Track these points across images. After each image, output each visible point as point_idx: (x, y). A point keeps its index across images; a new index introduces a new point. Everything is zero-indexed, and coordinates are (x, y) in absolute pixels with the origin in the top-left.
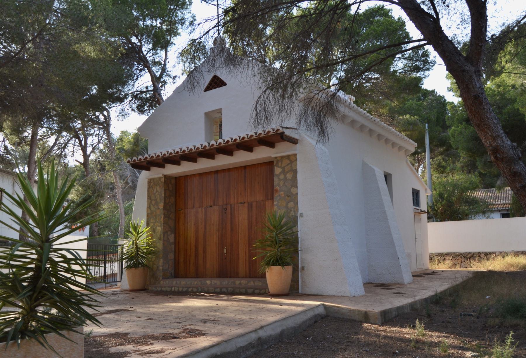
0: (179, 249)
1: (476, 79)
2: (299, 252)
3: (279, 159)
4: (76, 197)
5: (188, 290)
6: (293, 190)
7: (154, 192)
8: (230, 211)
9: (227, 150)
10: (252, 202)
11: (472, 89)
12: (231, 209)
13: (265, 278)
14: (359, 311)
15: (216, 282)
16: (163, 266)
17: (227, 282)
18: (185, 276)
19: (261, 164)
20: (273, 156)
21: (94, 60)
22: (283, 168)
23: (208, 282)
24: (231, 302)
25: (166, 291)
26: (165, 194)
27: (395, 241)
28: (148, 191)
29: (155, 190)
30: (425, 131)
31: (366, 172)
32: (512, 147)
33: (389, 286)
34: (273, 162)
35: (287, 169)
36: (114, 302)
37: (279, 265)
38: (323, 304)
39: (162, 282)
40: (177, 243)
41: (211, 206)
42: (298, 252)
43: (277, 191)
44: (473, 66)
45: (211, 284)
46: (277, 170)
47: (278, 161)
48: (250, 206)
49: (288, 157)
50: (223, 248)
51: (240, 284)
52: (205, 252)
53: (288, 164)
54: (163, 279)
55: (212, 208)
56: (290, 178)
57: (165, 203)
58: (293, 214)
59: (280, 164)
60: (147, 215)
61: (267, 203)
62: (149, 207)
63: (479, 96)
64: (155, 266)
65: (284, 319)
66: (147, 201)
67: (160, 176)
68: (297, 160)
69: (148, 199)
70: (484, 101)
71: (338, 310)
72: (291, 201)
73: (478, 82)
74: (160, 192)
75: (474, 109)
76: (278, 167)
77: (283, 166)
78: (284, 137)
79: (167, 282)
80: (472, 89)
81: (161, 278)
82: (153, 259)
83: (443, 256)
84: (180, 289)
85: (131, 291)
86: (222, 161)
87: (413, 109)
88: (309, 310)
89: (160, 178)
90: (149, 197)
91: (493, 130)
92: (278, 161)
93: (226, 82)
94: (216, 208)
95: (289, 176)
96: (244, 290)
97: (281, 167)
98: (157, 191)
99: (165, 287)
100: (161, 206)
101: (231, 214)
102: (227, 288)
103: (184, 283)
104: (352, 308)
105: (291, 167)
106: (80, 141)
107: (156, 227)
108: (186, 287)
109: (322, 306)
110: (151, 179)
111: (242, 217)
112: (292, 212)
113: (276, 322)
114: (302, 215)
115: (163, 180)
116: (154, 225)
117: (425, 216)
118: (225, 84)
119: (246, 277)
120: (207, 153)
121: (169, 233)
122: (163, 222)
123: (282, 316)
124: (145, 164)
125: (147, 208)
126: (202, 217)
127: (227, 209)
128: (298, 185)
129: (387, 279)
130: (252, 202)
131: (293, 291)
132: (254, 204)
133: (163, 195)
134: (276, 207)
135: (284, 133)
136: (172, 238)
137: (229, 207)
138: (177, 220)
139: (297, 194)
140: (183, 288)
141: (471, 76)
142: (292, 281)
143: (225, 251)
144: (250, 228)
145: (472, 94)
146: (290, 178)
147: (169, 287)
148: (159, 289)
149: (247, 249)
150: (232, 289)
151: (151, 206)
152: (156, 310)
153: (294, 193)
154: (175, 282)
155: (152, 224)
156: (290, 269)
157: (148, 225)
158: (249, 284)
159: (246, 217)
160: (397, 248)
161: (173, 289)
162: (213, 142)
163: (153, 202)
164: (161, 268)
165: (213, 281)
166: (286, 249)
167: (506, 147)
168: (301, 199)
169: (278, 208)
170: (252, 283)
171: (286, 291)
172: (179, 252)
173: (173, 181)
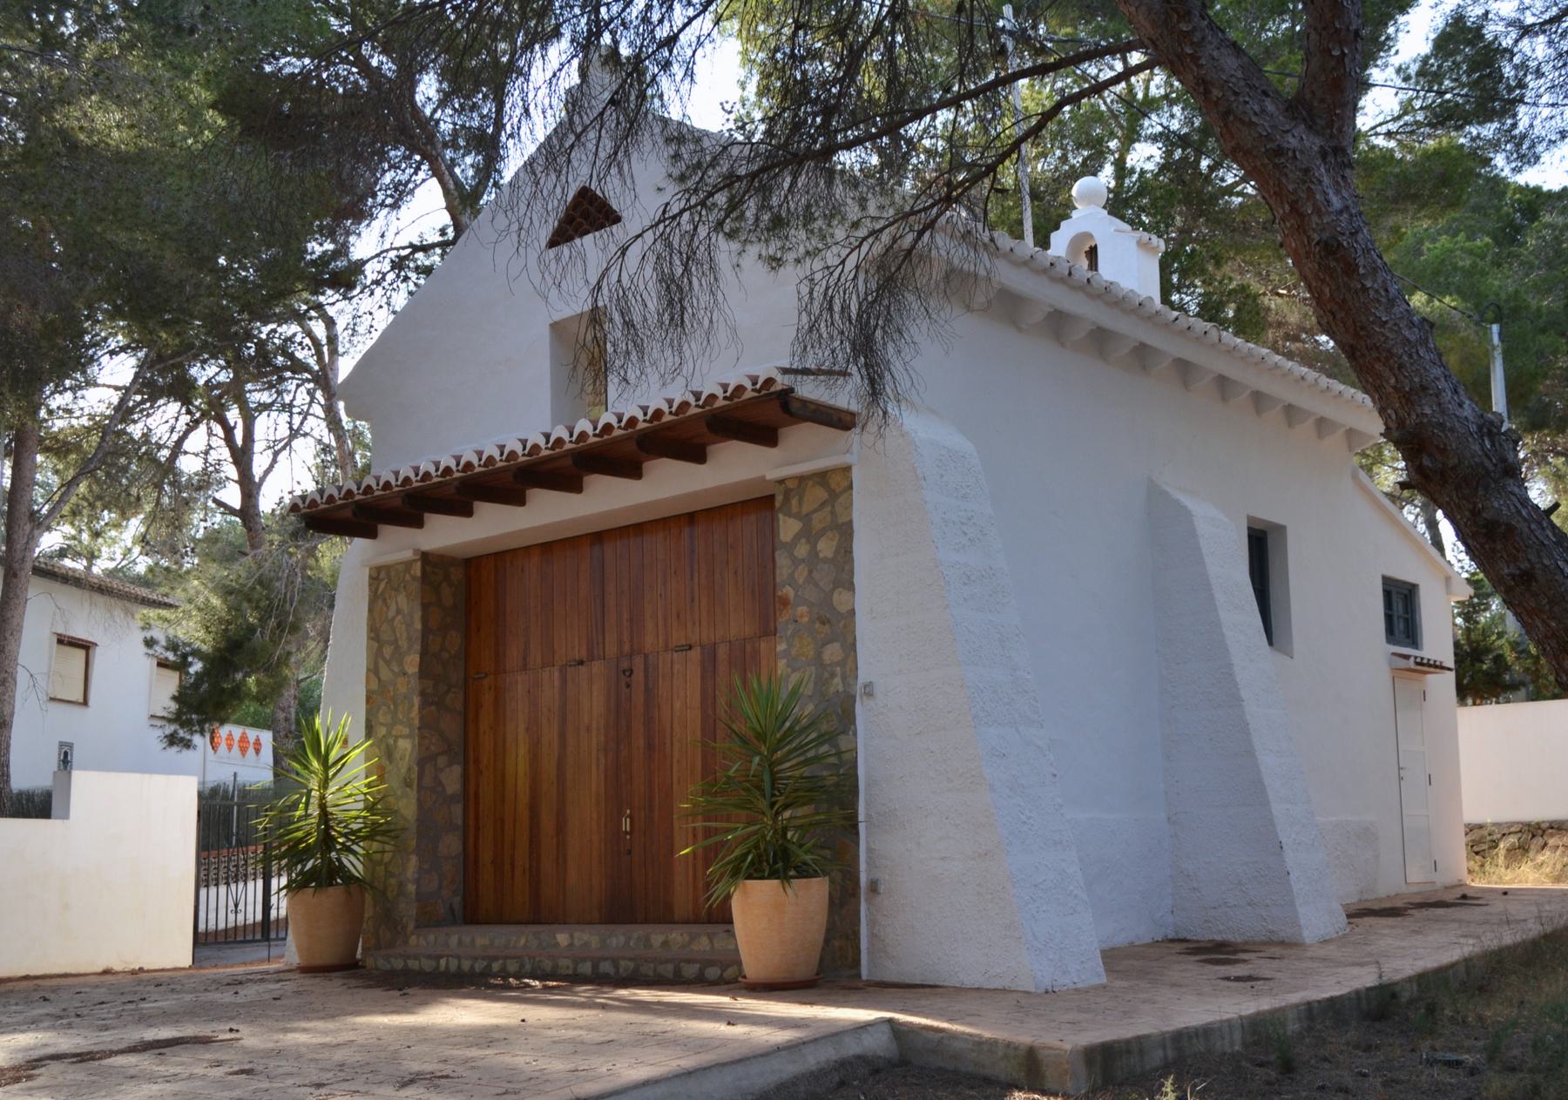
0: (477, 819)
1: (1326, 180)
2: (862, 827)
3: (790, 484)
4: (201, 634)
5: (489, 966)
6: (840, 599)
7: (391, 614)
9: (622, 454)
11: (1315, 219)
12: (646, 669)
13: (731, 922)
14: (1009, 1045)
15: (586, 937)
16: (417, 882)
17: (622, 939)
19: (744, 503)
20: (773, 474)
21: (120, 158)
22: (806, 519)
23: (562, 938)
24: (601, 1014)
25: (421, 973)
27: (1267, 781)
28: (371, 610)
29: (393, 608)
30: (1488, 355)
31: (1165, 526)
32: (1480, 428)
33: (1236, 952)
34: (771, 498)
35: (818, 521)
36: (167, 1017)
37: (773, 875)
38: (890, 1021)
39: (413, 940)
40: (469, 797)
41: (581, 663)
42: (855, 826)
43: (785, 602)
44: (1317, 133)
45: (571, 945)
46: (788, 528)
47: (787, 494)
49: (822, 477)
50: (620, 814)
51: (665, 944)
52: (561, 830)
53: (823, 505)
54: (417, 927)
55: (583, 669)
56: (830, 554)
57: (424, 654)
58: (841, 689)
59: (794, 502)
62: (373, 671)
63: (1340, 245)
64: (393, 881)
65: (689, 1074)
66: (369, 648)
67: (408, 555)
68: (851, 487)
69: (369, 638)
70: (1361, 261)
71: (940, 1041)
73: (1337, 192)
74: (407, 609)
75: (1327, 291)
76: (790, 515)
77: (805, 510)
78: (795, 406)
79: (431, 938)
80: (1315, 219)
81: (411, 926)
82: (387, 857)
83: (1532, 836)
84: (466, 965)
85: (307, 970)
86: (607, 498)
87: (1456, 268)
88: (815, 1040)
89: (408, 565)
90: (374, 633)
91: (1401, 367)
92: (787, 494)
94: (597, 667)
95: (826, 547)
96: (670, 967)
97: (797, 516)
99: (416, 957)
100: (412, 663)
101: (647, 689)
102: (615, 962)
103: (480, 941)
104: (987, 1034)
105: (833, 513)
106: (229, 431)
107: (397, 738)
108: (484, 958)
109: (886, 1028)
110: (379, 569)
112: (837, 680)
113: (646, 1084)
114: (869, 691)
115: (417, 570)
116: (389, 733)
117: (1445, 684)
120: (560, 469)
121: (442, 761)
122: (416, 722)
123: (688, 1062)
124: (348, 513)
126: (554, 705)
128: (856, 580)
129: (1236, 925)
131: (833, 968)
132: (722, 651)
133: (418, 626)
134: (782, 664)
135: (791, 390)
136: (452, 779)
137: (638, 663)
138: (469, 715)
139: (852, 612)
140: (476, 959)
141: (1306, 171)
142: (831, 931)
143: (626, 825)
145: (1316, 237)
146: (830, 554)
147: (429, 957)
148: (398, 964)
150: (631, 965)
151: (381, 663)
152: (302, 1038)
153: (843, 609)
154: (454, 940)
155: (382, 731)
156: (814, 893)
157: (370, 731)
158: (695, 947)
159: (695, 699)
160: (1277, 809)
161: (443, 962)
162: (583, 425)
164: (411, 888)
165: (577, 934)
166: (804, 812)
167: (1452, 430)
168: (864, 628)
169: (788, 666)
170: (704, 940)
171: (805, 971)
172: (477, 829)
173: (457, 574)
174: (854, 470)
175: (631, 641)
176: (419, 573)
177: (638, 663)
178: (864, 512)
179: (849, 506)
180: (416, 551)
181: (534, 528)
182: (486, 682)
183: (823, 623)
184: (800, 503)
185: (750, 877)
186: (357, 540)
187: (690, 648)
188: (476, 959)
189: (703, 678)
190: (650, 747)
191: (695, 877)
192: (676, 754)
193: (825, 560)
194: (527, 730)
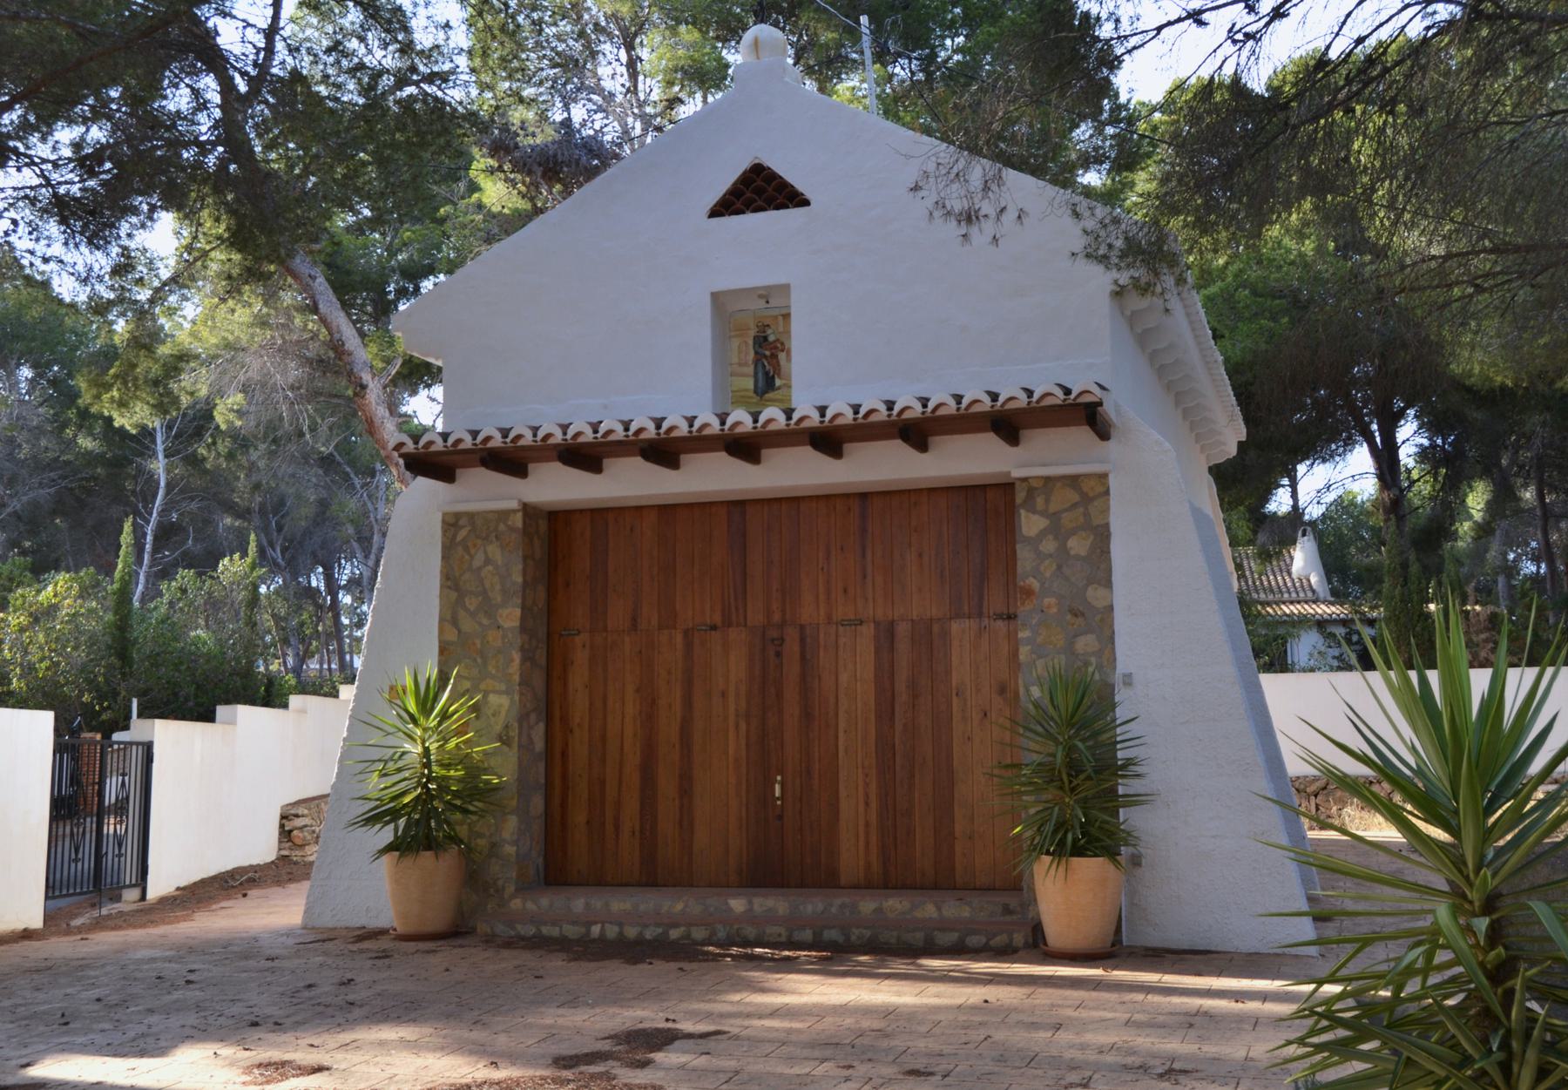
3: (1034, 484)
5: (666, 933)
6: (1095, 595)
8: (797, 648)
10: (892, 623)
12: (802, 640)
17: (820, 907)
18: (599, 880)
19: (948, 488)
20: (1017, 473)
22: (1055, 517)
26: (524, 573)
35: (1067, 520)
41: (714, 628)
43: (1028, 593)
46: (1030, 524)
47: (1031, 492)
48: (886, 634)
49: (1073, 481)
53: (1075, 506)
59: (1040, 501)
60: (442, 651)
62: (450, 619)
64: (482, 842)
67: (514, 505)
68: (1107, 492)
72: (1086, 633)
74: (504, 567)
76: (1034, 512)
77: (1053, 508)
79: (545, 902)
81: (511, 889)
84: (631, 932)
89: (504, 515)
92: (1031, 492)
93: (808, 195)
95: (1078, 545)
96: (920, 935)
97: (1044, 514)
98: (488, 561)
100: (511, 616)
103: (679, 907)
105: (1086, 515)
108: (658, 925)
110: (458, 515)
111: (851, 671)
114: (1128, 680)
115: (518, 521)
118: (805, 203)
119: (867, 885)
121: (533, 717)
122: (517, 678)
125: (442, 620)
127: (783, 640)
130: (892, 623)
132: (902, 630)
139: (1111, 608)
144: (885, 711)
149: (873, 786)
151: (462, 613)
153: (1100, 604)
163: (472, 603)
168: (1122, 623)
171: (436, 923)
175: (783, 611)
176: (519, 524)
177: (792, 634)
182: (578, 640)
184: (1047, 501)
185: (1072, 855)
186: (420, 479)
187: (861, 623)
188: (646, 926)
189: (877, 652)
190: (807, 715)
191: (867, 844)
192: (842, 726)
193: (1078, 557)
194: (637, 691)
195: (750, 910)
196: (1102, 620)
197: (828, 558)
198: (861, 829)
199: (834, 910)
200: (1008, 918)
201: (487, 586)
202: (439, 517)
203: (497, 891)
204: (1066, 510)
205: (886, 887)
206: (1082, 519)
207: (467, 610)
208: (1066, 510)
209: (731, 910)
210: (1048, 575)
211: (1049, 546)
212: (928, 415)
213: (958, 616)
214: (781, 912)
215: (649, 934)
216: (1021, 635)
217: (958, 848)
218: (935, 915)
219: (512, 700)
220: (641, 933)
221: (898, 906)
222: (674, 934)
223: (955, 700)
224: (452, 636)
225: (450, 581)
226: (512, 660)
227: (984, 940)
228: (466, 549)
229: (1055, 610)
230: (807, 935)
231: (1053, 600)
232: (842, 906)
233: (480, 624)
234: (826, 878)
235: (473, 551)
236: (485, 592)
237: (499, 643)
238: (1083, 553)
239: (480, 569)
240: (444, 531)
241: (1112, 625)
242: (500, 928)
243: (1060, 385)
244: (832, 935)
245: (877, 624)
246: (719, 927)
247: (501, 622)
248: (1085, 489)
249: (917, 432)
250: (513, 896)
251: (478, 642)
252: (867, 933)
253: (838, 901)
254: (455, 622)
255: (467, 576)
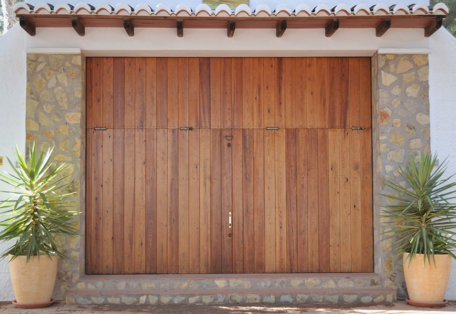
3: (389, 57)
5: (187, 300)
6: (420, 118)
7: (50, 85)
12: (244, 137)
17: (269, 283)
41: (191, 129)
43: (385, 116)
46: (386, 79)
47: (387, 61)
49: (410, 57)
53: (410, 70)
59: (392, 67)
61: (330, 133)
62: (32, 117)
68: (427, 64)
74: (71, 87)
76: (389, 72)
77: (399, 71)
81: (76, 277)
89: (69, 57)
94: (205, 134)
95: (412, 92)
97: (394, 74)
102: (293, 295)
103: (185, 285)
105: (417, 75)
108: (182, 295)
110: (38, 56)
115: (79, 61)
125: (27, 118)
132: (302, 135)
139: (429, 125)
151: (41, 114)
153: (423, 123)
163: (48, 109)
168: (434, 133)
171: (45, 299)
174: (429, 56)
178: (434, 78)
179: (427, 74)
180: (82, 51)
181: (202, 51)
183: (411, 129)
184: (396, 67)
193: (411, 98)
195: (229, 286)
196: (424, 132)
197: (259, 93)
198: (278, 241)
199: (277, 285)
200: (374, 287)
201: (58, 99)
202: (25, 56)
203: (67, 278)
204: (406, 73)
205: (291, 272)
206: (414, 78)
207: (44, 112)
208: (406, 73)
209: (217, 286)
210: (396, 106)
211: (396, 91)
212: (33, 13)
213: (332, 127)
214: (246, 287)
215: (176, 301)
216: (381, 138)
217: (332, 252)
218: (334, 287)
219: (76, 167)
220: (171, 300)
221: (314, 282)
222: (192, 300)
223: (330, 172)
224: (35, 127)
225: (33, 94)
226: (76, 143)
227: (371, 299)
228: (43, 76)
229: (399, 125)
230: (272, 299)
231: (399, 120)
232: (282, 282)
233: (54, 121)
234: (257, 268)
235: (48, 78)
236: (57, 102)
237: (67, 133)
238: (415, 96)
239: (53, 88)
240: (29, 65)
241: (429, 134)
242: (81, 300)
243: (69, 5)
244: (300, 297)
245: (287, 130)
246: (220, 295)
247: (67, 120)
248: (416, 62)
249: (331, 25)
250: (78, 282)
251: (53, 132)
252: (306, 297)
253: (280, 280)
254: (36, 119)
255: (44, 92)
